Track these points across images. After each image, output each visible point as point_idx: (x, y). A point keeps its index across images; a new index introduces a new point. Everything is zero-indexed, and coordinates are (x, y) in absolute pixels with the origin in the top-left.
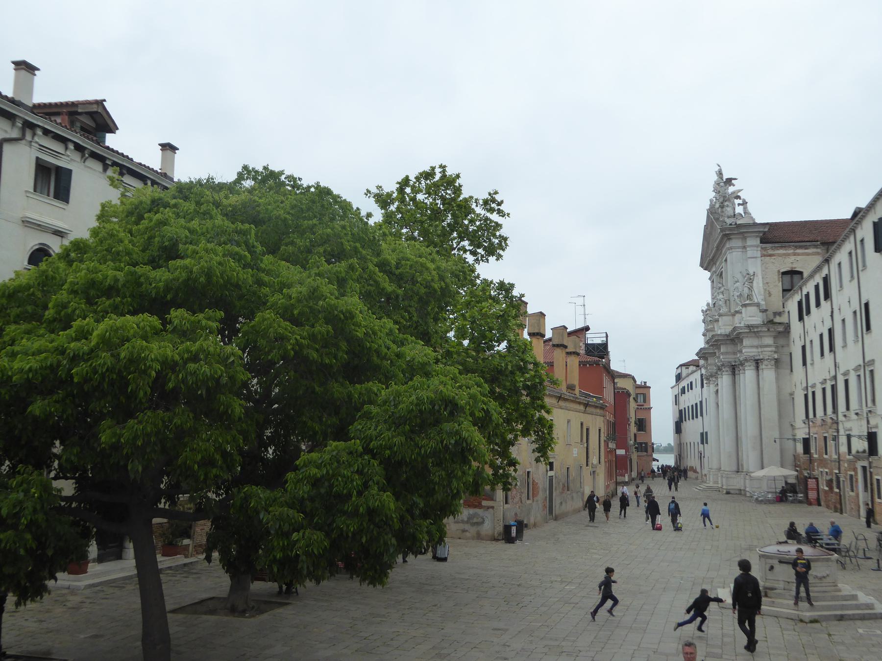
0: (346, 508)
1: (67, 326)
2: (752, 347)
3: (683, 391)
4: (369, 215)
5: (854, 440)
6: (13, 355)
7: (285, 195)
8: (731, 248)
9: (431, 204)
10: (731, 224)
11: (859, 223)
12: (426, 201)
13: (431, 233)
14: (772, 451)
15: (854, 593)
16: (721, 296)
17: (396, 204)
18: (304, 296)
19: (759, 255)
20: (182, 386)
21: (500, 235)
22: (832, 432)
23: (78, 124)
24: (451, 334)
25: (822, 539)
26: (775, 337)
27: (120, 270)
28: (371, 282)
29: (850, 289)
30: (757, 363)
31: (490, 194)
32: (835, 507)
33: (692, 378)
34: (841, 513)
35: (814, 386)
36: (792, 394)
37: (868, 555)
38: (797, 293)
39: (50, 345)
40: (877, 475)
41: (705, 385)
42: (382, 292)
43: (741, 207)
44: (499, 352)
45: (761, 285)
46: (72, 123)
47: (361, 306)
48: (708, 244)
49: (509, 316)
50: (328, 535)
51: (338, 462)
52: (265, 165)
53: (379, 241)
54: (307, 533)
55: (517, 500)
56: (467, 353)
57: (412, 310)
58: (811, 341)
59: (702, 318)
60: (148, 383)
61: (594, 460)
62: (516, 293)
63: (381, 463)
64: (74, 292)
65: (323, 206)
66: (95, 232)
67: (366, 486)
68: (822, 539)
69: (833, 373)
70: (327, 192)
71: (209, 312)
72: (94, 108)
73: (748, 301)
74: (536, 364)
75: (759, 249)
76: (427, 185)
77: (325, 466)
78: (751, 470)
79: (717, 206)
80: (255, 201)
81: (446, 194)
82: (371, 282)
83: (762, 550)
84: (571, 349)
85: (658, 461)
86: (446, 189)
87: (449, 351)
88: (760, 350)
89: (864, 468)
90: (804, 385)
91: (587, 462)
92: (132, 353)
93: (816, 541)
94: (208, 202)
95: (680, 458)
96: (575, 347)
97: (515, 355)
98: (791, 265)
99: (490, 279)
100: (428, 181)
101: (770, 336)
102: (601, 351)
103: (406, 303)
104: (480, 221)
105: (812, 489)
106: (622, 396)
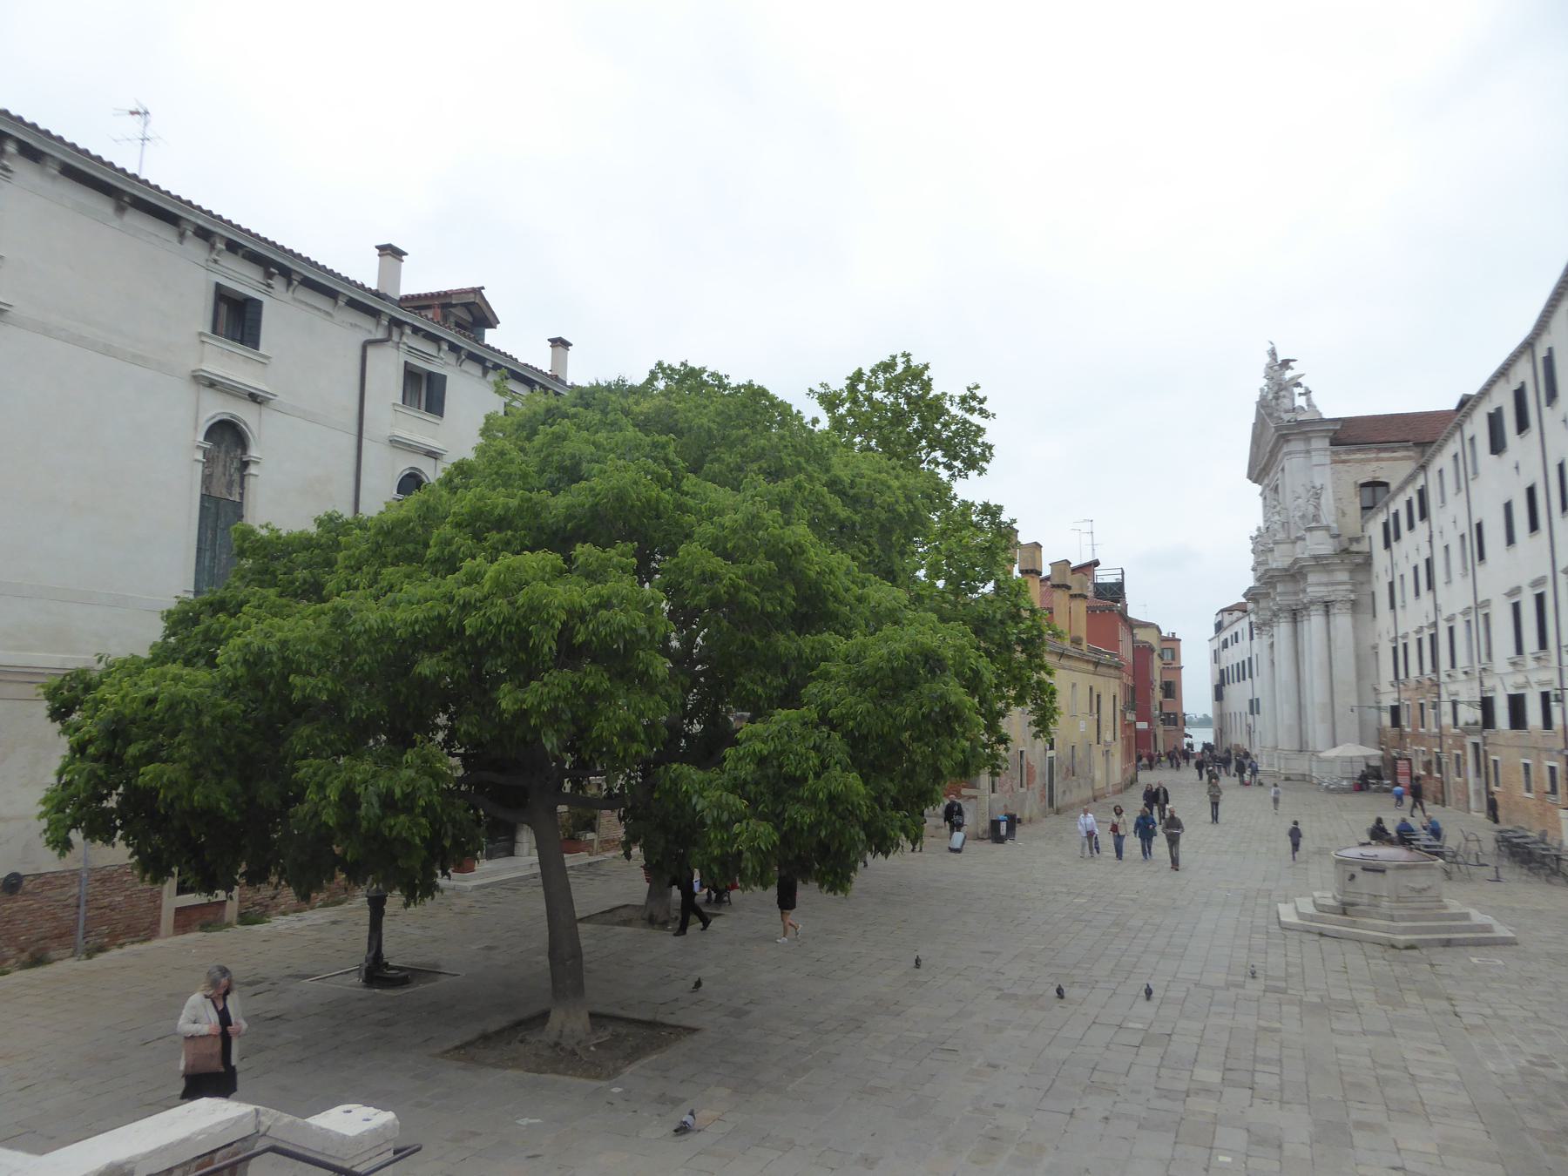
0: (801, 793)
1: (454, 570)
2: (1319, 584)
3: (1225, 644)
4: (815, 421)
5: (1462, 709)
6: (394, 605)
7: (709, 397)
8: (1289, 453)
9: (892, 404)
10: (1289, 421)
11: (1468, 415)
12: (885, 400)
13: (893, 442)
14: (1347, 724)
15: (1463, 911)
16: (1276, 518)
17: (847, 405)
18: (741, 525)
19: (1329, 462)
20: (594, 638)
21: (983, 443)
22: (1431, 697)
23: (452, 319)
24: (921, 573)
25: (1418, 840)
26: (1351, 572)
27: (513, 496)
28: (820, 507)
29: (1456, 505)
30: (1327, 606)
31: (969, 389)
32: (1435, 797)
33: (1237, 628)
34: (1444, 805)
35: (1405, 636)
36: (1375, 647)
37: (1482, 861)
38: (1382, 511)
39: (436, 591)
40: (1495, 754)
41: (1255, 636)
42: (833, 519)
43: (1303, 398)
44: (984, 595)
45: (1332, 502)
46: (445, 318)
47: (812, 538)
48: (1258, 447)
49: (997, 548)
50: (777, 828)
51: (789, 736)
52: (684, 361)
53: (827, 453)
54: (751, 824)
55: (1006, 787)
56: (943, 598)
57: (872, 541)
58: (1402, 576)
59: (1251, 547)
60: (553, 636)
61: (1107, 736)
62: (1004, 518)
63: (843, 736)
64: (458, 525)
65: (755, 412)
66: (481, 451)
67: (824, 766)
68: (1418, 840)
69: (1432, 619)
70: (763, 392)
71: (620, 546)
72: (471, 298)
73: (1313, 523)
74: (1033, 611)
75: (1328, 453)
76: (886, 379)
77: (772, 739)
78: (1319, 749)
79: (1270, 396)
80: (672, 407)
81: (912, 390)
82: (820, 507)
83: (1339, 853)
84: (1074, 591)
85: (1191, 737)
86: (912, 383)
87: (918, 594)
88: (1330, 588)
89: (1476, 745)
90: (1392, 635)
91: (1098, 738)
92: (531, 599)
93: (1410, 842)
94: (615, 410)
95: (1221, 733)
96: (1082, 588)
97: (1005, 599)
98: (1372, 474)
99: (970, 501)
100: (888, 375)
101: (1346, 570)
102: (1115, 592)
103: (865, 532)
104: (957, 424)
105: (1404, 774)
106: (1143, 653)
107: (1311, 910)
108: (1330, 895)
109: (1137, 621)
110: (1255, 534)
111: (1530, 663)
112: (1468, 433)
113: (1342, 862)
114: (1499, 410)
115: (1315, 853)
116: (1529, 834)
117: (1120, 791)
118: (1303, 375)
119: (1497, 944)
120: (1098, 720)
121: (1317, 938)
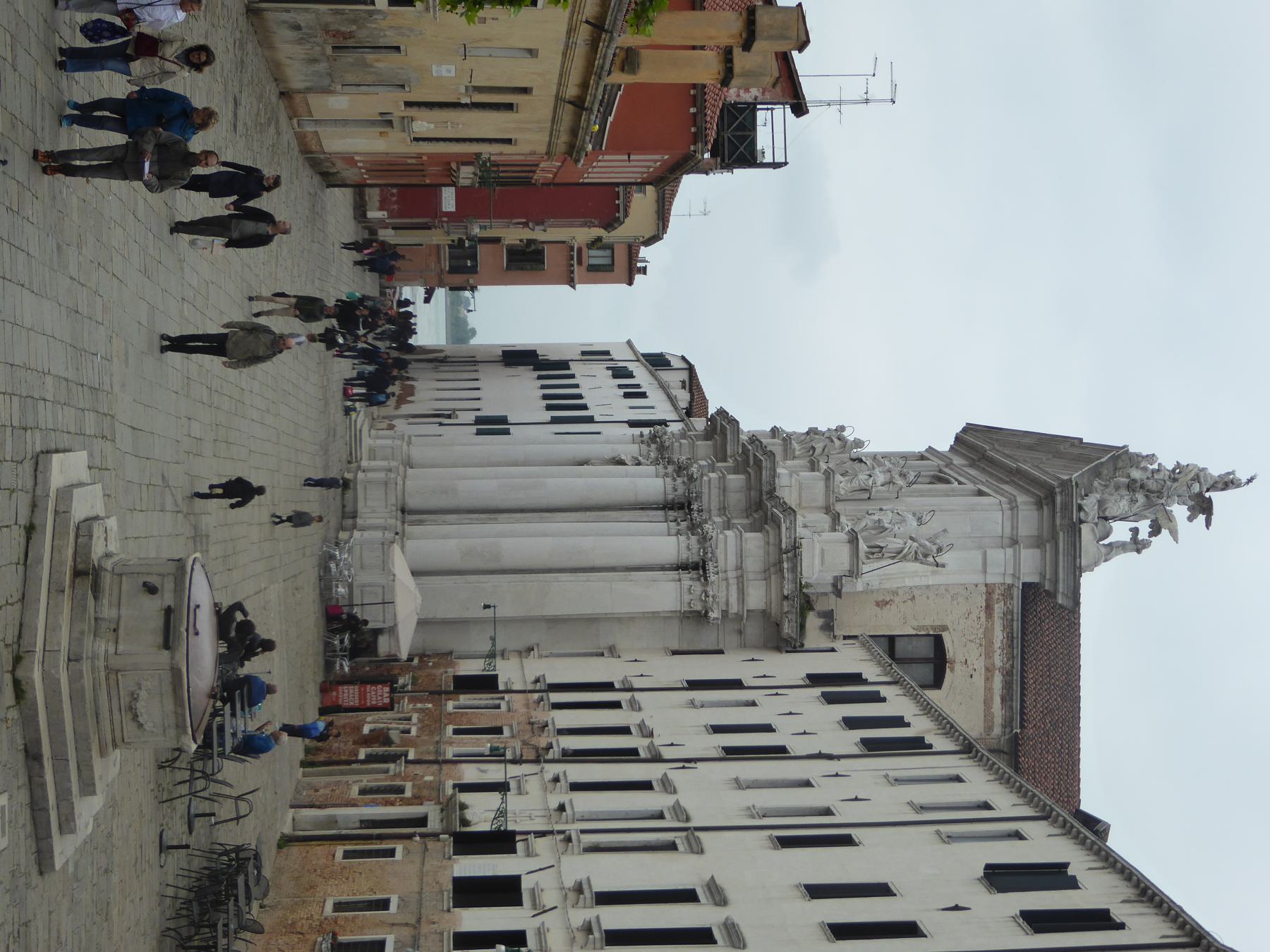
2: (741, 555)
3: (620, 373)
5: (494, 799)
8: (1014, 506)
10: (1080, 508)
11: (1067, 830)
15: (99, 786)
19: (990, 580)
25: (233, 715)
26: (765, 614)
30: (697, 567)
34: (304, 764)
35: (635, 706)
36: (613, 651)
40: (407, 851)
41: (637, 431)
43: (1126, 537)
45: (909, 582)
48: (1030, 448)
58: (753, 704)
59: (822, 428)
61: (424, 124)
68: (233, 715)
75: (1009, 581)
79: (1136, 474)
83: (198, 567)
84: (741, 60)
85: (427, 300)
88: (732, 574)
89: (422, 821)
90: (637, 683)
95: (436, 360)
96: (747, 74)
101: (769, 603)
105: (363, 696)
107: (80, 510)
108: (112, 548)
109: (673, 195)
110: (849, 435)
111: (579, 916)
112: (1030, 829)
113: (180, 570)
114: (1072, 884)
115: (196, 528)
116: (255, 904)
117: (305, 150)
118: (1176, 539)
119: (38, 839)
120: (456, 105)
121: (23, 521)
